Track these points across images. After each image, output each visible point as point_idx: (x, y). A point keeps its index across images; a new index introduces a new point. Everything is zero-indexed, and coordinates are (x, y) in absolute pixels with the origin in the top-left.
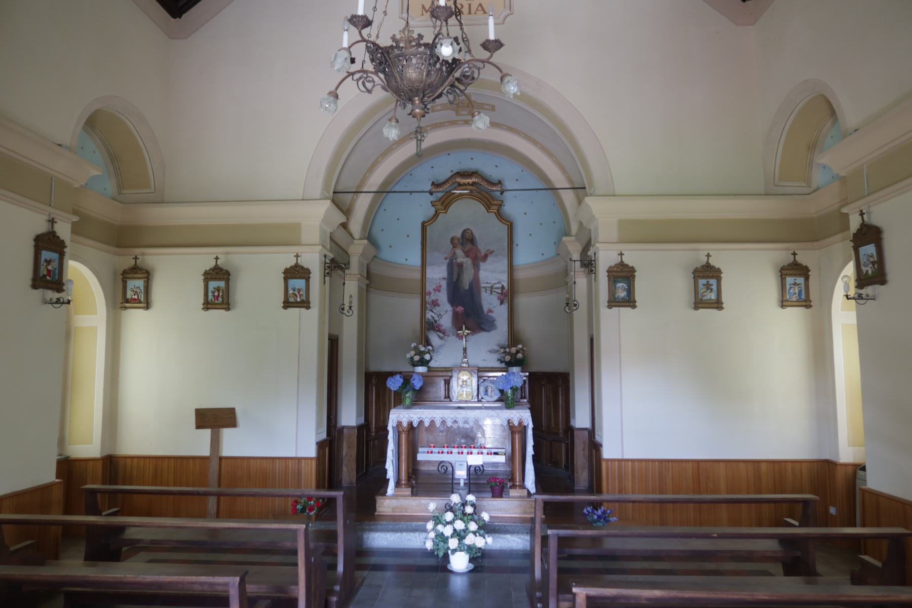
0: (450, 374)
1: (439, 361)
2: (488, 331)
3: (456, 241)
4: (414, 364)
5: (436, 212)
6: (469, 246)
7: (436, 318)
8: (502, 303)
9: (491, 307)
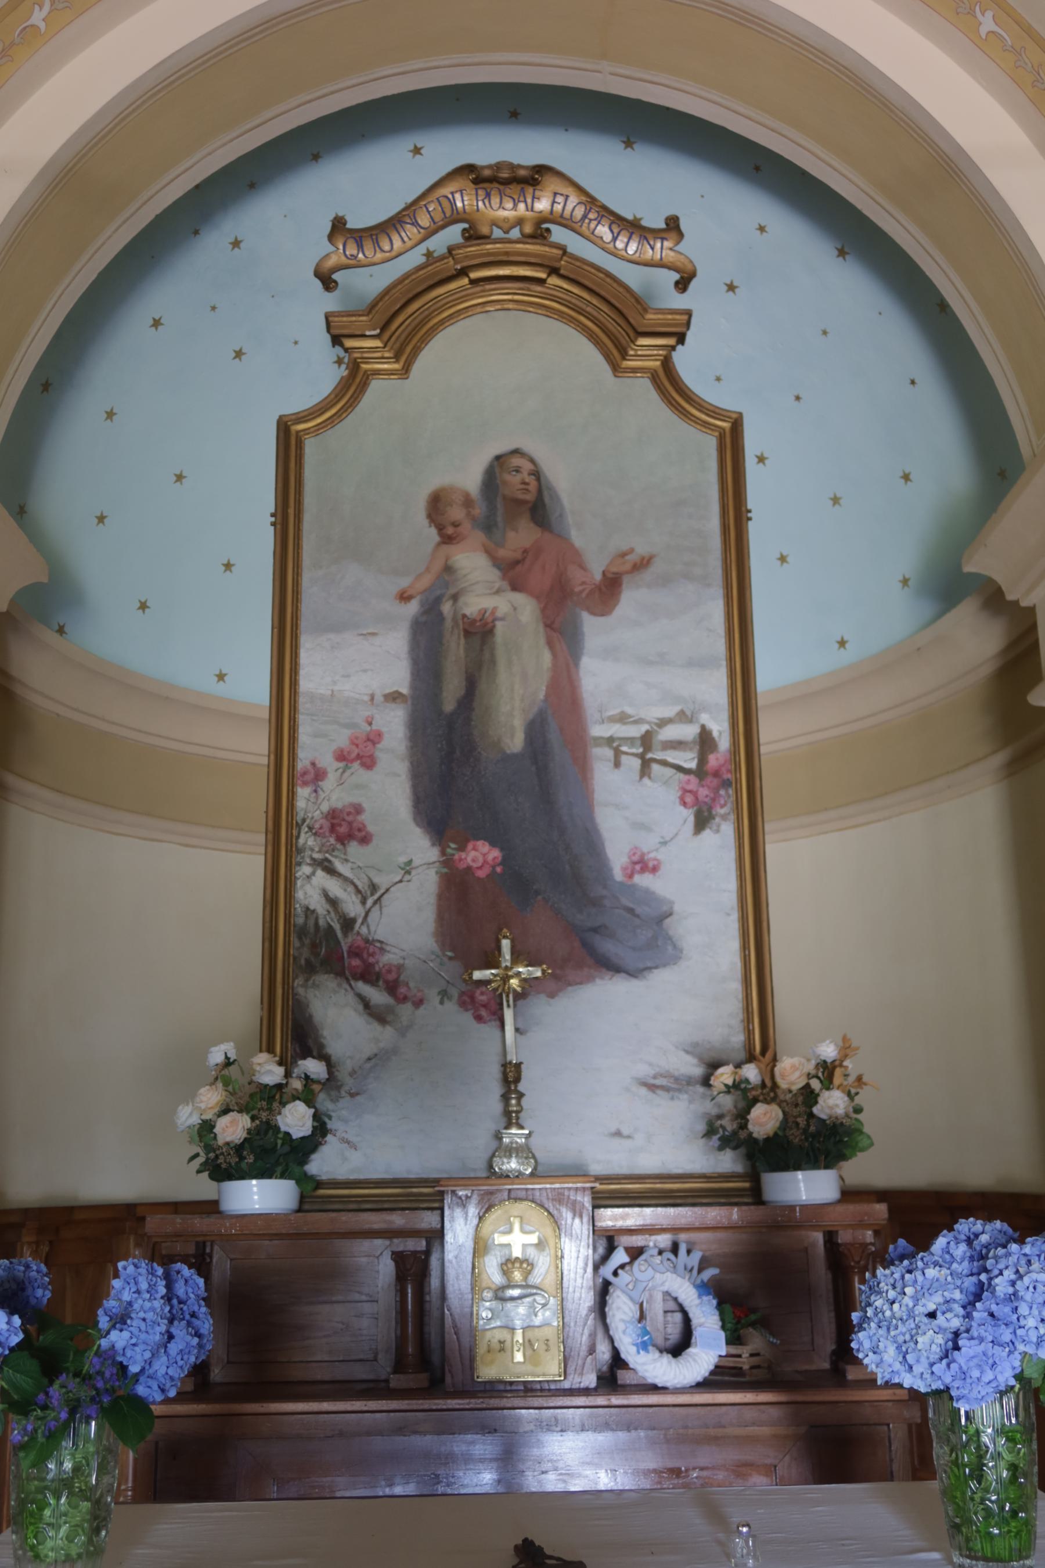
0: (428, 1220)
1: (361, 1150)
2: (634, 974)
3: (456, 513)
4: (225, 1166)
5: (354, 367)
6: (522, 536)
7: (352, 907)
8: (702, 822)
9: (648, 844)
